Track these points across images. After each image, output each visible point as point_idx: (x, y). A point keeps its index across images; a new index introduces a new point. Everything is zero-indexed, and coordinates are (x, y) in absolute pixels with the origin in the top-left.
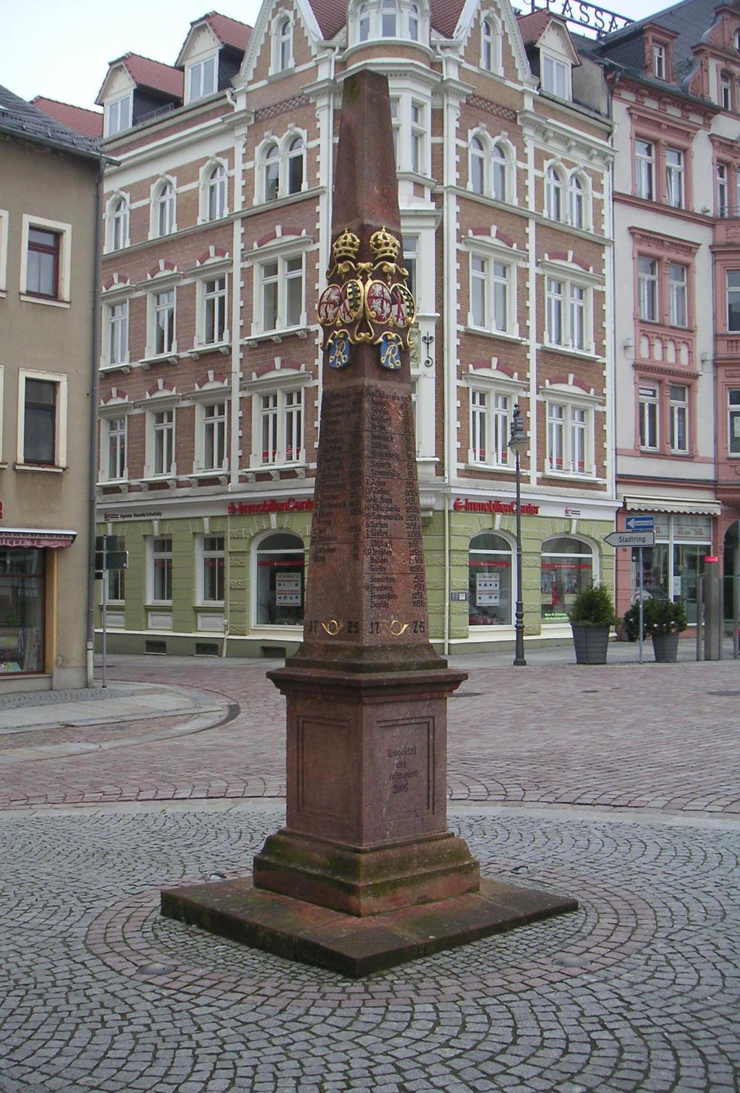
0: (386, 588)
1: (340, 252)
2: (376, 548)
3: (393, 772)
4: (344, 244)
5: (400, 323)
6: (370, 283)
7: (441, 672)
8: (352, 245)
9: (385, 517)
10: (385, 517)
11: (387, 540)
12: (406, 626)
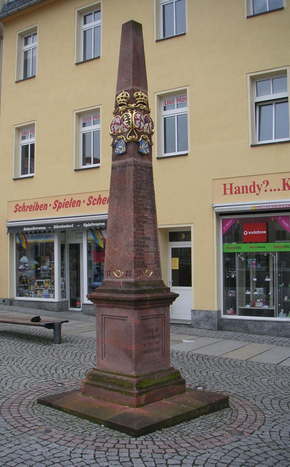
1: (120, 102)
4: (122, 98)
5: (148, 131)
6: (134, 113)
7: (168, 294)
8: (126, 98)
12: (152, 272)
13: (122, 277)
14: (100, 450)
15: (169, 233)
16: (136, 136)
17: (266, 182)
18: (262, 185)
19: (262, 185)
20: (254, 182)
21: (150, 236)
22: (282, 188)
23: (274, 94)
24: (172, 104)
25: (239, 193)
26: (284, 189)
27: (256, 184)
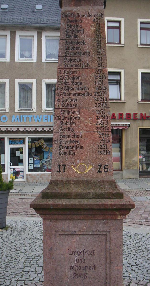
0: (73, 142)
2: (66, 115)
3: (73, 265)
9: (75, 95)
10: (75, 95)
11: (75, 110)
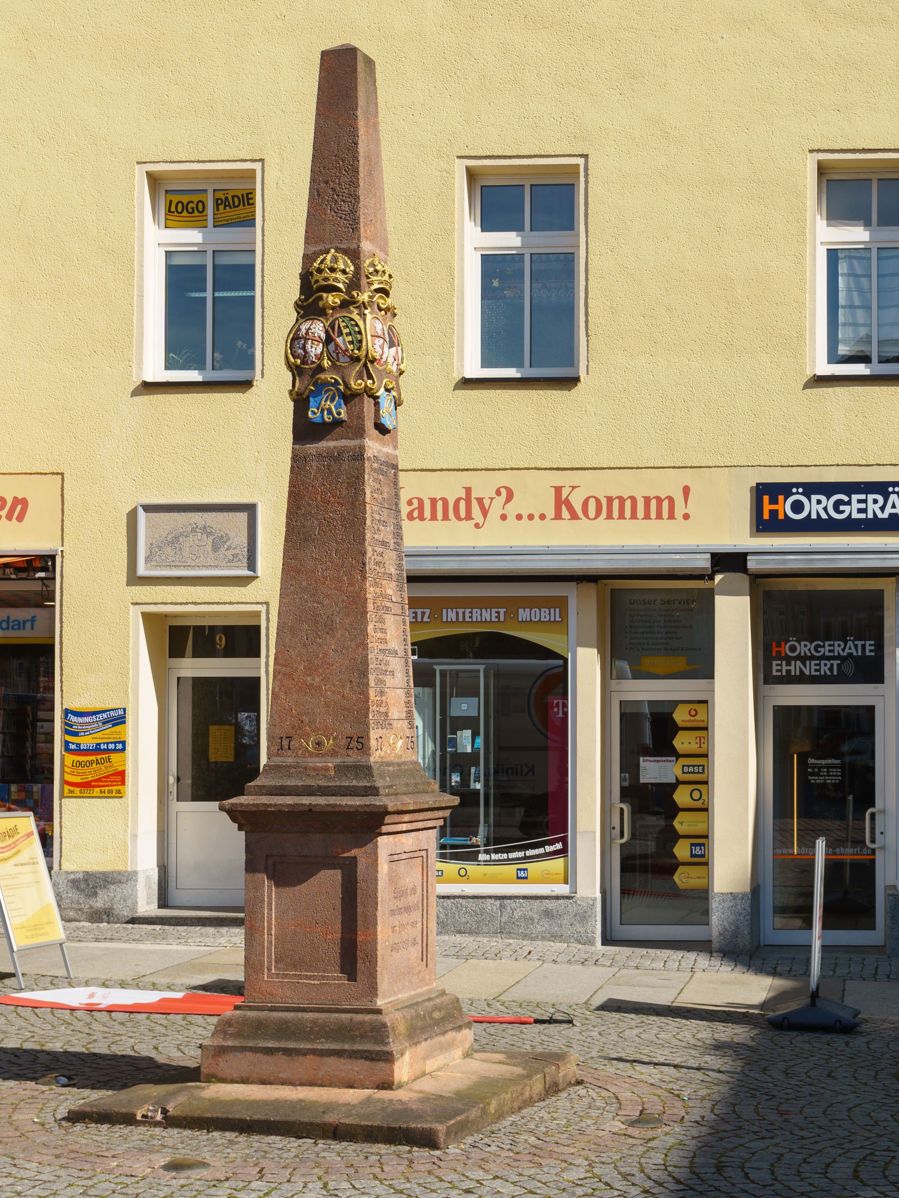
13: (333, 753)
14: (672, 1070)
15: (170, 627)
16: (374, 383)
17: (503, 491)
18: (492, 499)
19: (492, 499)
20: (468, 490)
21: (396, 648)
22: (551, 514)
23: (533, 233)
24: (196, 213)
25: (421, 518)
26: (558, 516)
27: (474, 495)
